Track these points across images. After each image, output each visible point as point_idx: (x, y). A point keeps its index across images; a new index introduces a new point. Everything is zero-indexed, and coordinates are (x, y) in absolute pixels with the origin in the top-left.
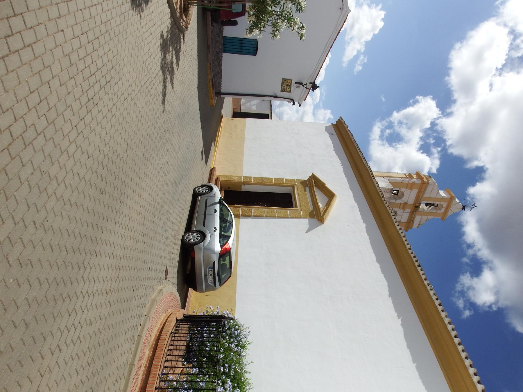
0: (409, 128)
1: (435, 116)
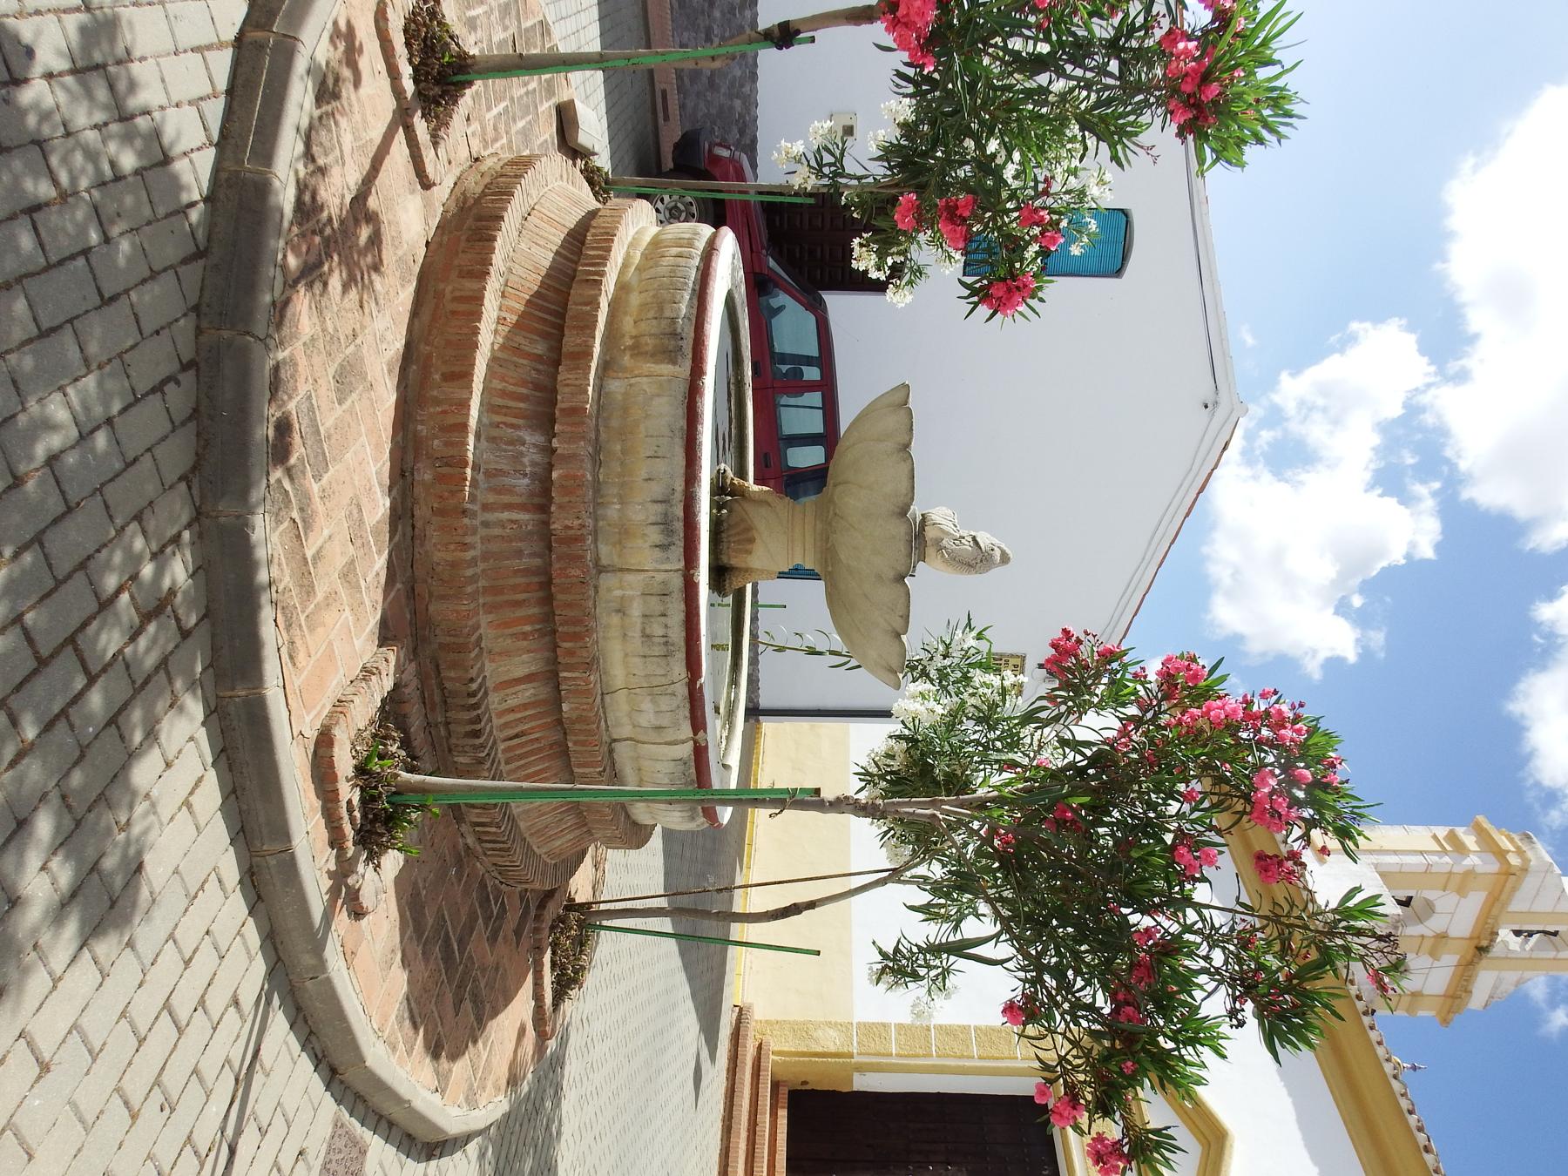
0: (1336, 422)
1: (1419, 382)
